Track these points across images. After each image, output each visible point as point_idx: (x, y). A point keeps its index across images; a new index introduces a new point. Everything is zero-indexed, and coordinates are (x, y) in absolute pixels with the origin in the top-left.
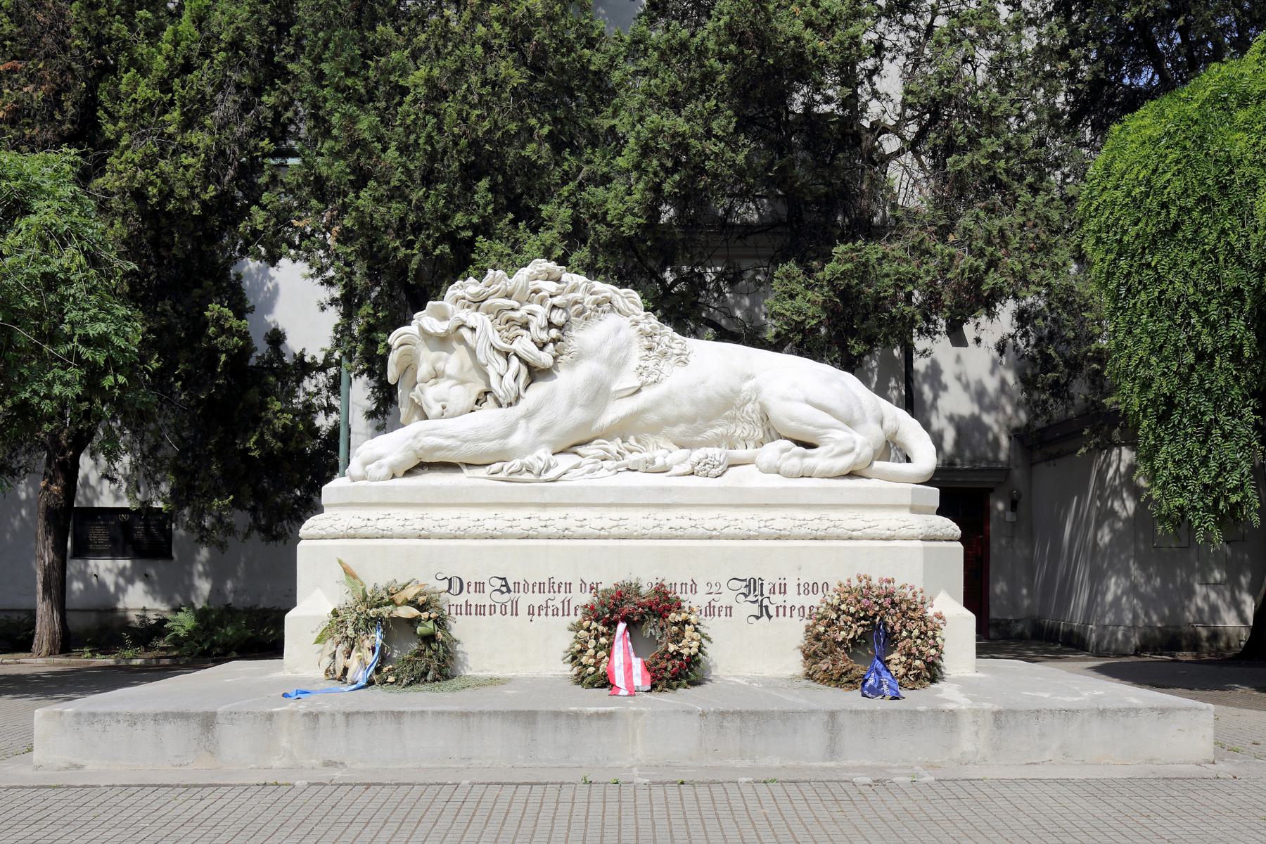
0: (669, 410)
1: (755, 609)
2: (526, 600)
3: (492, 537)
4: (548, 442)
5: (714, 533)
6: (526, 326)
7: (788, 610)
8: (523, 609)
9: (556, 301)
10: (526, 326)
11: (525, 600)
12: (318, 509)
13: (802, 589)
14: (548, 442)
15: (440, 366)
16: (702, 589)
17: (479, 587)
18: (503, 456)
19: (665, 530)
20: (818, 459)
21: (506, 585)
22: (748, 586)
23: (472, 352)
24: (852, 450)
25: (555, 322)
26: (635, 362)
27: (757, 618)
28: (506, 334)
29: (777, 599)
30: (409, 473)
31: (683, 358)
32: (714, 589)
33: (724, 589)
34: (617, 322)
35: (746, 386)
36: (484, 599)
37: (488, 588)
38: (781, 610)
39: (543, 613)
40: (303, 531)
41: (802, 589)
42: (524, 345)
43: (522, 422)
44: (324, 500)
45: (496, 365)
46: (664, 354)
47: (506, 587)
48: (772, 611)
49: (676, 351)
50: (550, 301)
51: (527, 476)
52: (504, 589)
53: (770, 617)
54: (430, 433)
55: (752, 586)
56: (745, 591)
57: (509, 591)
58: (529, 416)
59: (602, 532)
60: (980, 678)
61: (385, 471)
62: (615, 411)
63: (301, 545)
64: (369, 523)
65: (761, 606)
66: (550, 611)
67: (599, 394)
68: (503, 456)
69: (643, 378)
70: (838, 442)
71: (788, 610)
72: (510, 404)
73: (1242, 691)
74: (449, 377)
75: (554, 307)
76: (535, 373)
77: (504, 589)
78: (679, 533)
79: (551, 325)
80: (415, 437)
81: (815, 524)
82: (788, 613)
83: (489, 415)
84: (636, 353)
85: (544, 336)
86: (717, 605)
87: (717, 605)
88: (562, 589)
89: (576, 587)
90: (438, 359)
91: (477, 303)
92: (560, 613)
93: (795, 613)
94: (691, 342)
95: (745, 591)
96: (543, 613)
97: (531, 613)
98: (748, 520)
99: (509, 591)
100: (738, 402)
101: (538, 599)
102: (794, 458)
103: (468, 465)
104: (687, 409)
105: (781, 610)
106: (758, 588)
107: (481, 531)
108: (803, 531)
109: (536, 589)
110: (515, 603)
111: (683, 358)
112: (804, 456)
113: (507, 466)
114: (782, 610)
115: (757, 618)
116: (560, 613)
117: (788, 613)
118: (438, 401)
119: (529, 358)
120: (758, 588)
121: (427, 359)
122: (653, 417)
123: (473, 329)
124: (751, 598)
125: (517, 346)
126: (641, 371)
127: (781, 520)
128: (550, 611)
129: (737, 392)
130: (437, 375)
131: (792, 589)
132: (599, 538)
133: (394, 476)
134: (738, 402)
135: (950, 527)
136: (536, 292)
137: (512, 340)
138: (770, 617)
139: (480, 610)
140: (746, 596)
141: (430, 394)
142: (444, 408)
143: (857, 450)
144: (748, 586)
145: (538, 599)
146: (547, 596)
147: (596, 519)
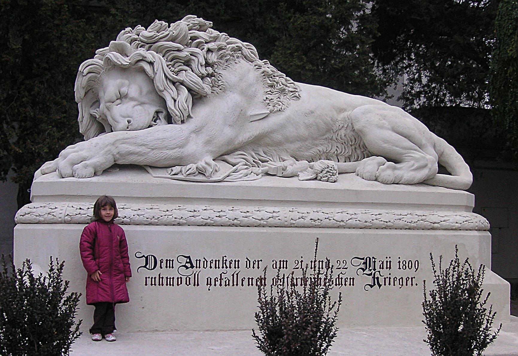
0: (291, 131)
2: (205, 274)
3: (179, 224)
4: (212, 152)
5: (342, 223)
6: (188, 63)
7: (392, 280)
8: (203, 281)
9: (211, 45)
10: (188, 63)
11: (205, 274)
13: (401, 265)
14: (212, 152)
15: (124, 90)
17: (169, 264)
18: (180, 162)
19: (307, 221)
20: (404, 171)
21: (190, 262)
22: (365, 263)
23: (151, 81)
24: (425, 166)
25: (210, 62)
26: (261, 96)
27: (371, 286)
28: (173, 69)
29: (385, 272)
30: (106, 171)
31: (297, 94)
32: (342, 265)
33: (349, 265)
34: (245, 70)
36: (173, 273)
37: (176, 265)
38: (387, 280)
39: (218, 283)
41: (401, 265)
42: (188, 76)
43: (193, 135)
45: (170, 91)
46: (282, 91)
47: (190, 264)
48: (381, 282)
49: (291, 89)
50: (206, 46)
51: (200, 178)
52: (189, 265)
53: (380, 286)
54: (124, 141)
55: (368, 263)
56: (363, 266)
57: (192, 267)
58: (197, 131)
59: (262, 222)
61: (91, 170)
62: (254, 130)
64: (82, 212)
65: (374, 277)
66: (223, 283)
67: (241, 118)
68: (180, 162)
69: (271, 107)
70: (417, 160)
71: (392, 280)
72: (183, 122)
74: (132, 99)
75: (209, 50)
76: (197, 97)
77: (189, 265)
78: (317, 223)
79: (207, 64)
80: (113, 144)
81: (408, 218)
82: (392, 283)
83: (162, 129)
84: (261, 92)
85: (203, 71)
86: (344, 277)
87: (344, 277)
88: (233, 265)
89: (242, 264)
90: (123, 85)
91: (149, 44)
92: (231, 284)
93: (397, 282)
94: (302, 87)
95: (363, 266)
96: (218, 283)
97: (209, 283)
98: (362, 214)
99: (192, 267)
100: (335, 128)
101: (215, 273)
102: (388, 171)
103: (151, 167)
104: (303, 132)
105: (387, 280)
106: (372, 264)
107: (171, 219)
108: (401, 223)
109: (213, 265)
111: (297, 94)
112: (395, 169)
113: (184, 169)
114: (389, 281)
115: (371, 286)
116: (231, 284)
117: (392, 283)
118: (124, 117)
119: (192, 85)
120: (372, 264)
121: (112, 85)
122: (278, 137)
123: (151, 63)
124: (367, 272)
125: (182, 77)
126: (267, 102)
127: (387, 215)
128: (223, 283)
129: (334, 121)
130: (122, 97)
131: (395, 265)
132: (259, 226)
133: (95, 174)
134: (335, 128)
135: (481, 220)
136: (193, 39)
137: (177, 74)
138: (380, 286)
139: (170, 282)
140: (364, 270)
141: (119, 112)
142: (129, 122)
143: (429, 165)
144: (365, 263)
145: (215, 273)
146: (221, 270)
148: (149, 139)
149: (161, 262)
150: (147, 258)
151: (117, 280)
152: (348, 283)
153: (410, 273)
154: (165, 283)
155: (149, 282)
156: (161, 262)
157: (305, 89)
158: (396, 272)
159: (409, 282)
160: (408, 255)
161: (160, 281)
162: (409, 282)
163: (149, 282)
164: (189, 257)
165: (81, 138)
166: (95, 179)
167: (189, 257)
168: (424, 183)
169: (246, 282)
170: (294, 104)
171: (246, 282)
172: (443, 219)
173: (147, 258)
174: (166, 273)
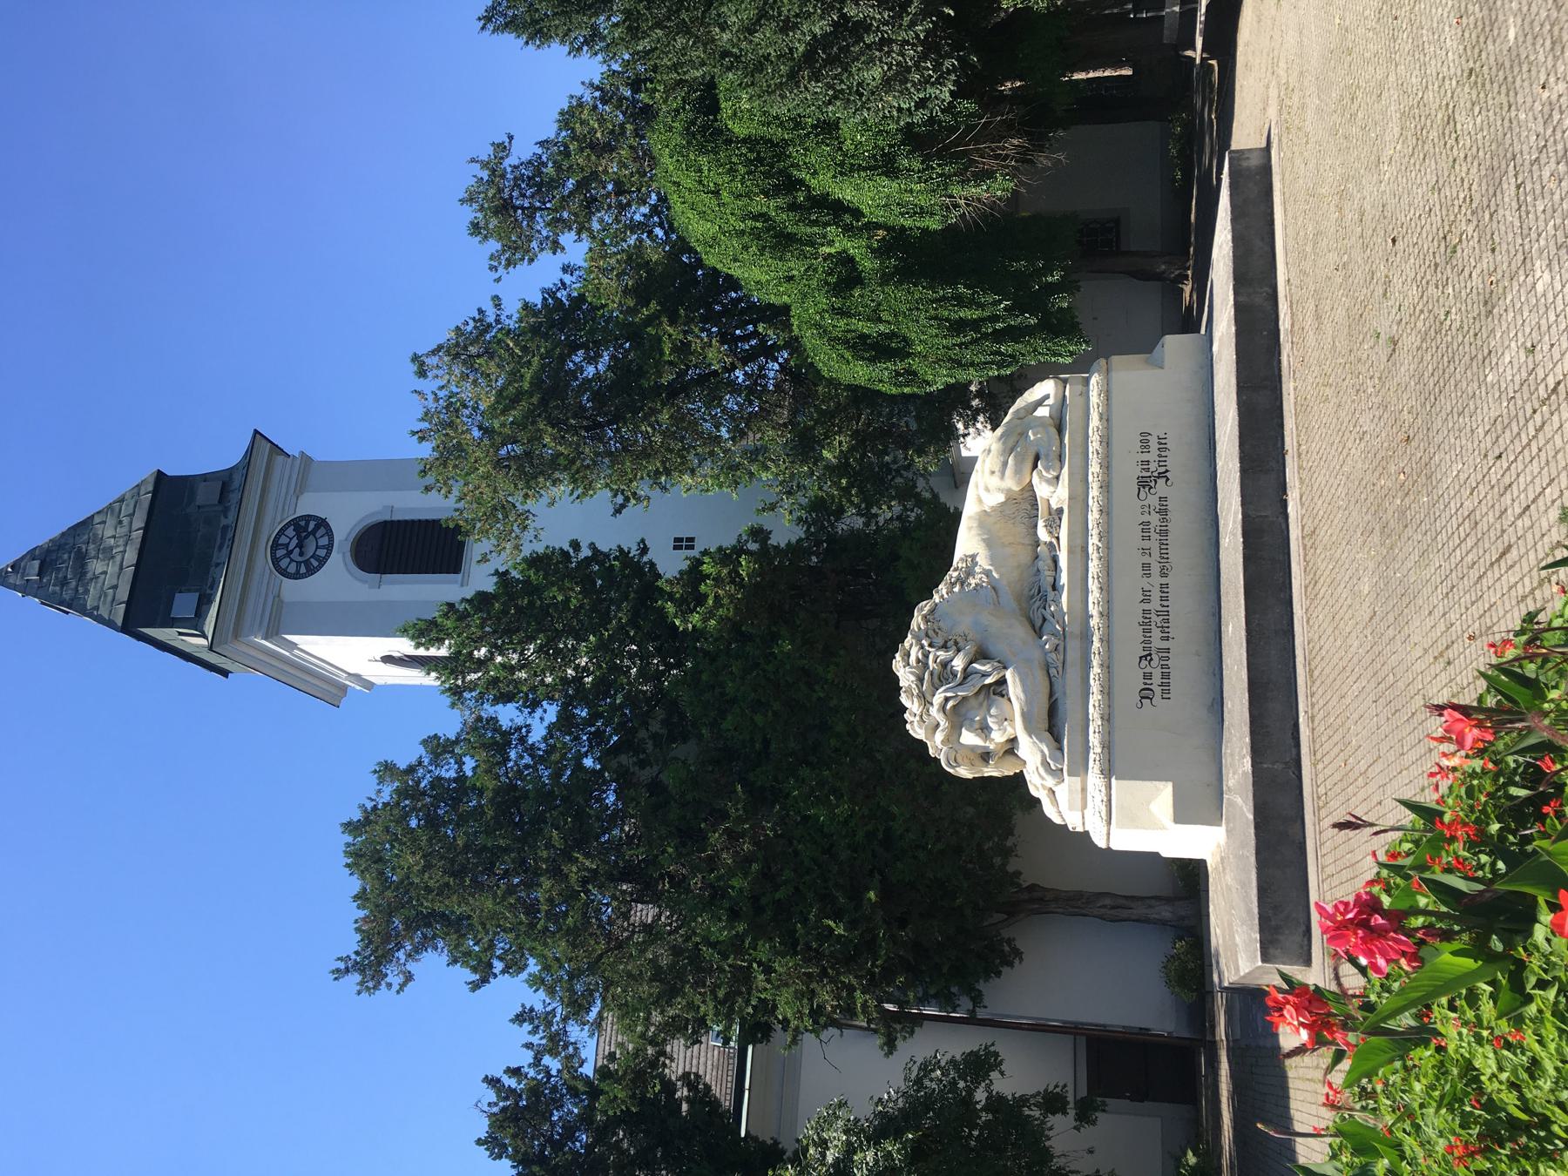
1: (1161, 481)
8: (1165, 645)
11: (1157, 643)
12: (1086, 833)
16: (1146, 518)
29: (1153, 466)
30: (1058, 739)
35: (394, 978)
37: (1148, 670)
40: (1102, 844)
44: (1080, 829)
47: (1147, 657)
55: (1144, 483)
60: (1070, 474)
63: (1115, 846)
73: (1233, 329)
89: (1146, 606)
101: (1156, 633)
110: (1159, 650)
131: (1145, 457)
145: (1156, 633)
147: (1094, 594)
158: (1152, 456)
174: (1157, 679)
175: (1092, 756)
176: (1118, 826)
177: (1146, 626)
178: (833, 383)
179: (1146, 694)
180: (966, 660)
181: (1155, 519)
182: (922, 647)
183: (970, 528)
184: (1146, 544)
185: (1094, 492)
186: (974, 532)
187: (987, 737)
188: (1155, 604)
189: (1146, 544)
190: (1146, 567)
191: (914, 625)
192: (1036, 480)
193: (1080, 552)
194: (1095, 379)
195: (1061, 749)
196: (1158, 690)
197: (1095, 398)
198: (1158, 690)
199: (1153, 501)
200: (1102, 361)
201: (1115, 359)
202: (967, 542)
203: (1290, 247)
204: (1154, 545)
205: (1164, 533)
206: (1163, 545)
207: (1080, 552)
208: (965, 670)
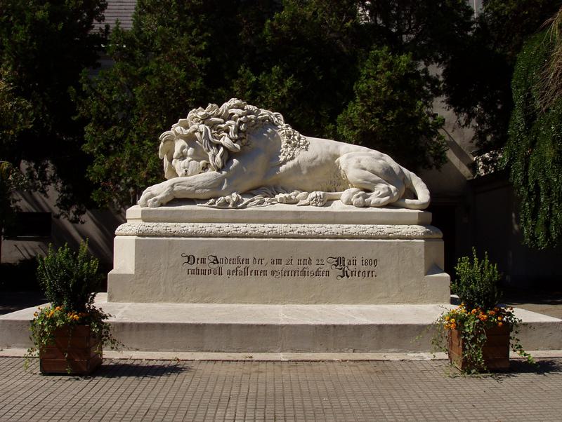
8: (225, 273)
17: (203, 261)
21: (217, 260)
27: (342, 277)
29: (352, 267)
30: (169, 204)
32: (320, 262)
39: (235, 274)
47: (216, 261)
55: (339, 261)
56: (336, 263)
57: (218, 263)
87: (322, 270)
93: (361, 274)
95: (336, 263)
96: (235, 274)
97: (229, 273)
99: (218, 263)
101: (232, 267)
114: (354, 273)
115: (342, 277)
124: (338, 267)
128: (238, 273)
139: (203, 272)
144: (337, 261)
145: (232, 267)
146: (237, 265)
148: (195, 182)
149: (198, 259)
150: (189, 257)
151: (479, 264)
152: (286, 274)
153: (372, 268)
154: (200, 273)
155: (190, 272)
156: (198, 259)
157: (313, 141)
158: (360, 267)
159: (370, 274)
160: (369, 255)
161: (197, 272)
162: (370, 274)
163: (190, 272)
164: (216, 257)
165: (166, 180)
166: (160, 208)
167: (216, 257)
168: (389, 205)
169: (253, 273)
170: (303, 153)
171: (253, 273)
172: (396, 230)
173: (189, 257)
174: (201, 266)
175: (205, 225)
176: (136, 240)
177: (238, 260)
178: (518, 49)
179: (190, 259)
180: (226, 145)
181: (314, 267)
182: (240, 117)
183: (328, 147)
184: (295, 262)
185: (267, 228)
186: (324, 150)
187: (177, 158)
188: (252, 267)
189: (295, 262)
190: (279, 261)
191: (263, 111)
192: (353, 190)
193: (298, 218)
194: (421, 230)
195: (162, 205)
196: (194, 267)
197: (404, 229)
198: (194, 267)
199: (326, 267)
200: (441, 235)
201: (442, 243)
202: (318, 146)
203: (316, 366)
204: (294, 266)
205: (303, 273)
206: (294, 273)
207: (298, 218)
208: (222, 145)
